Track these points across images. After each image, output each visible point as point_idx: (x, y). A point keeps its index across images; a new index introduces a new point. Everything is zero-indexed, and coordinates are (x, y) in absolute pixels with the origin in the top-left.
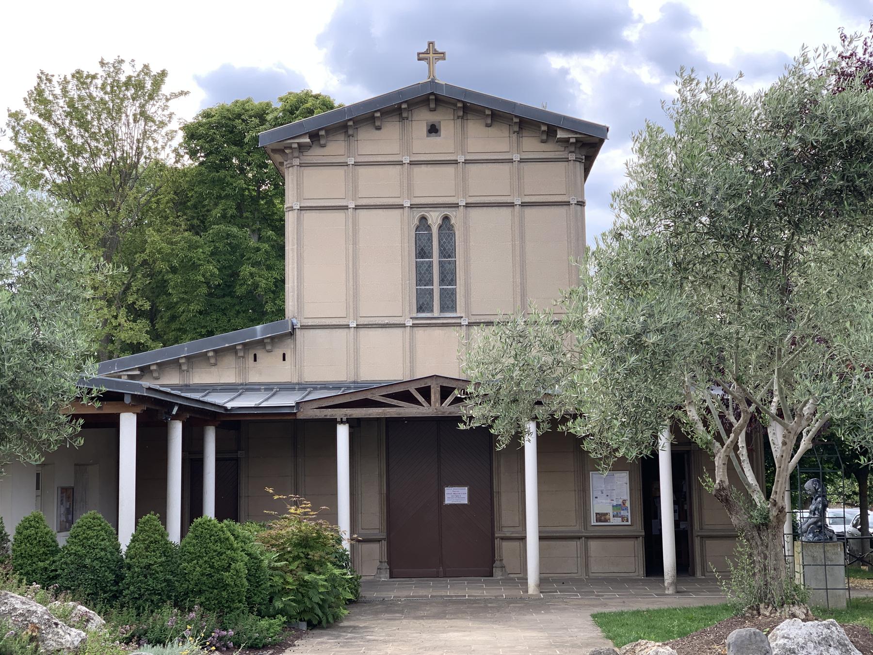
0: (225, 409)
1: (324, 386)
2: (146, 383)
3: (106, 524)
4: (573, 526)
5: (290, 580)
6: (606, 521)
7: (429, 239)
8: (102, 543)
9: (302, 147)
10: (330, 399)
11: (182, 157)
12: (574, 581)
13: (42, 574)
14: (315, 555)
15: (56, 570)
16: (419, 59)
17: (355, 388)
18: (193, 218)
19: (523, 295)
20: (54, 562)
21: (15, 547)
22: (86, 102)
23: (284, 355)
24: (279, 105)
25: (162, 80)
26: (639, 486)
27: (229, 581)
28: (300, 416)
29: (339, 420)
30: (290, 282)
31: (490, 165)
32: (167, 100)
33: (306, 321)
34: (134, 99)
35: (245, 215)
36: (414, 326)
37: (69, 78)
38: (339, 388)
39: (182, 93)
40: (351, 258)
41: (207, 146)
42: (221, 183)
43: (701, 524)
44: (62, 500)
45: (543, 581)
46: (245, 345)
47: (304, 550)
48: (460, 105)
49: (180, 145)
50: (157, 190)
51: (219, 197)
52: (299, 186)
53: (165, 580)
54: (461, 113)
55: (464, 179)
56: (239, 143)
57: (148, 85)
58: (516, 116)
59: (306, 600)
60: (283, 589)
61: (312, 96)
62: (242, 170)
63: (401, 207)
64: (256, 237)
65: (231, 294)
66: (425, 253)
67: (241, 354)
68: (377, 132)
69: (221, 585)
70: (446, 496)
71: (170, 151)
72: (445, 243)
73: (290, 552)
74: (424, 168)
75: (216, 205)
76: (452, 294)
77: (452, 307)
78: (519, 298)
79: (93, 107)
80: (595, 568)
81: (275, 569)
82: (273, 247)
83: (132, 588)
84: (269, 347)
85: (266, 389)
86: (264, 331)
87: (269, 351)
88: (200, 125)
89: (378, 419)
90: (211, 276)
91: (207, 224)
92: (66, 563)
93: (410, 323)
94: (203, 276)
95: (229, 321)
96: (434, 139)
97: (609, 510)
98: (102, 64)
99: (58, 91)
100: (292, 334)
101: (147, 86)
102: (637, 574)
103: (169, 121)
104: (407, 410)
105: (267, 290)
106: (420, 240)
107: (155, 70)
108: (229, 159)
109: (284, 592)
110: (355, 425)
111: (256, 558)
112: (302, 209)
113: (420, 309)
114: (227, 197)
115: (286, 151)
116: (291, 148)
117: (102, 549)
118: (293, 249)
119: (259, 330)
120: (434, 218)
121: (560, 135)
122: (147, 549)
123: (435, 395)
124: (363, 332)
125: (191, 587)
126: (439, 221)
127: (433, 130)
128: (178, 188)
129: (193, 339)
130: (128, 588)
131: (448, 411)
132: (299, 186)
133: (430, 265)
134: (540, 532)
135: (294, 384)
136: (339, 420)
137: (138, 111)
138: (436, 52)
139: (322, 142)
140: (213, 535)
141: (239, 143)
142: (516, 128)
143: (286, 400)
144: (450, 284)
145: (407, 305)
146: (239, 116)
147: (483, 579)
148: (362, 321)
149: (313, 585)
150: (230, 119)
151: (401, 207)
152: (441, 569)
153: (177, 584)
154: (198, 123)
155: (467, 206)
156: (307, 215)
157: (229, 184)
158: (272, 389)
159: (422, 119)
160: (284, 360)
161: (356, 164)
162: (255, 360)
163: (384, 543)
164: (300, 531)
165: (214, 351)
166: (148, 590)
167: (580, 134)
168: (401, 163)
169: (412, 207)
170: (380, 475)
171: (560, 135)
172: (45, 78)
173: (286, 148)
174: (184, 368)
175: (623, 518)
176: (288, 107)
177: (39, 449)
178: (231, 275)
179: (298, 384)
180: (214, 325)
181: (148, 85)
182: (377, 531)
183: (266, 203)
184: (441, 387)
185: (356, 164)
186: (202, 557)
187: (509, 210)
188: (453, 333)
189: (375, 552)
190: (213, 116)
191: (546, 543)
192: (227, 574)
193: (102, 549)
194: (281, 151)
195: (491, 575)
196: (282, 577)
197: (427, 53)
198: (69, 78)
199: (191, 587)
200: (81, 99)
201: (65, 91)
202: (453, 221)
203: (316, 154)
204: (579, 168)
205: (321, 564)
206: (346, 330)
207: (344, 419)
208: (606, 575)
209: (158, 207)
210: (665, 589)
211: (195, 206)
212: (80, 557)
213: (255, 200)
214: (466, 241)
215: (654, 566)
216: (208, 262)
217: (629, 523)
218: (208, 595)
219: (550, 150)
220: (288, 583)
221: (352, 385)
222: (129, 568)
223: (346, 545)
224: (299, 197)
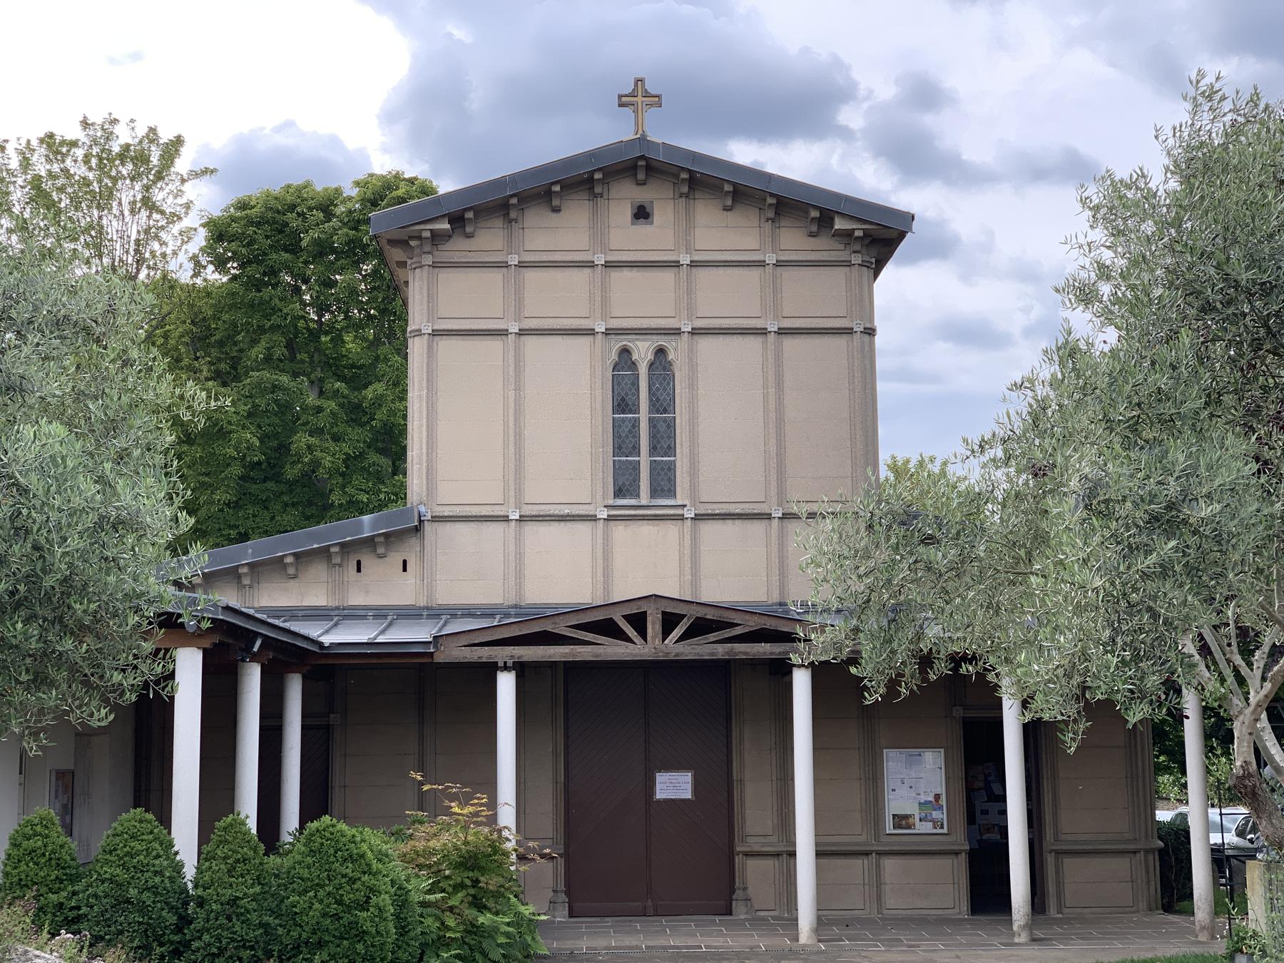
0: (321, 645)
1: (469, 612)
2: (228, 597)
3: (160, 831)
4: (857, 835)
5: (451, 922)
6: (909, 827)
7: (633, 384)
8: (157, 862)
9: (437, 238)
10: (489, 632)
11: (205, 267)
12: (860, 921)
13: (54, 915)
14: (491, 882)
15: (78, 908)
16: (621, 105)
17: (517, 615)
18: (219, 360)
20: (74, 893)
21: (8, 869)
22: (60, 182)
23: (405, 562)
24: (354, 192)
25: (177, 151)
26: (960, 772)
27: (368, 926)
28: (440, 658)
30: (416, 447)
31: (729, 271)
32: (183, 181)
33: (440, 509)
34: (133, 179)
35: (298, 357)
36: (610, 519)
37: (35, 143)
38: (492, 616)
40: (511, 411)
41: (244, 251)
42: (267, 309)
43: (1056, 834)
44: (57, 791)
45: (822, 923)
46: (343, 545)
47: (471, 874)
48: (684, 176)
50: (164, 318)
51: (262, 330)
52: (431, 298)
53: (261, 925)
54: (685, 189)
55: (690, 291)
56: (294, 248)
57: (155, 160)
58: (772, 195)
60: (439, 938)
61: (404, 179)
62: (297, 290)
63: (591, 332)
64: (316, 390)
65: (277, 477)
66: (627, 405)
67: (337, 560)
68: (554, 215)
69: (354, 932)
70: (658, 786)
71: (184, 257)
72: (658, 389)
73: (447, 878)
74: (626, 273)
75: (254, 342)
76: (669, 469)
77: (670, 490)
78: (773, 477)
79: (70, 190)
80: (891, 901)
82: (341, 406)
83: (206, 937)
84: (381, 550)
85: (375, 617)
86: (375, 525)
87: (381, 556)
89: (553, 664)
90: (248, 449)
91: (241, 371)
92: (95, 896)
93: (604, 514)
94: (236, 449)
95: (273, 518)
96: (642, 229)
98: (85, 124)
99: (14, 163)
100: (418, 529)
101: (151, 160)
102: (957, 910)
103: (187, 213)
105: (334, 472)
106: (619, 384)
107: (166, 136)
108: (273, 272)
110: (523, 670)
112: (436, 333)
113: (619, 493)
114: (274, 328)
115: (412, 243)
116: (420, 238)
117: (156, 873)
118: (420, 397)
119: (367, 523)
120: (643, 351)
121: (839, 224)
122: (230, 872)
124: (530, 528)
125: (304, 935)
126: (650, 356)
127: (642, 214)
128: (196, 314)
129: (216, 545)
130: (200, 938)
131: (674, 652)
132: (431, 298)
133: (635, 424)
134: (817, 844)
135: (420, 608)
137: (139, 197)
138: (647, 95)
139: (469, 229)
141: (294, 248)
142: (771, 214)
143: (418, 633)
144: (666, 455)
145: (600, 485)
146: (292, 207)
147: (717, 918)
148: (528, 510)
149: (492, 932)
150: (278, 212)
151: (591, 332)
152: (650, 903)
153: (280, 931)
154: (231, 217)
155: (695, 332)
156: (444, 344)
157: (275, 310)
158: (385, 617)
159: (624, 196)
160: (405, 570)
161: (522, 265)
162: (359, 570)
163: (561, 862)
164: (466, 843)
165: (295, 555)
166: (233, 940)
167: (871, 223)
168: (591, 265)
169: (608, 333)
171: (839, 224)
173: (411, 238)
174: (246, 581)
175: (935, 823)
176: (369, 195)
177: (106, 701)
178: (279, 450)
179: (427, 608)
180: (250, 523)
181: (155, 160)
183: (332, 340)
184: (664, 613)
185: (522, 265)
186: (322, 886)
187: (760, 339)
188: (672, 529)
189: (547, 874)
190: (253, 207)
191: (825, 861)
192: (365, 914)
193: (156, 873)
194: (403, 243)
195: (729, 912)
196: (437, 918)
198: (35, 143)
199: (304, 935)
200: (50, 174)
201: (26, 164)
202: (671, 356)
203: (457, 248)
207: (510, 664)
208: (909, 912)
209: (166, 342)
210: (1013, 935)
211: (221, 344)
212: (120, 885)
213: (314, 335)
214: (692, 386)
215: (988, 894)
216: (244, 427)
217: (945, 831)
218: (333, 949)
219: (824, 247)
220: (448, 928)
221: (512, 611)
222: (201, 903)
224: (432, 314)
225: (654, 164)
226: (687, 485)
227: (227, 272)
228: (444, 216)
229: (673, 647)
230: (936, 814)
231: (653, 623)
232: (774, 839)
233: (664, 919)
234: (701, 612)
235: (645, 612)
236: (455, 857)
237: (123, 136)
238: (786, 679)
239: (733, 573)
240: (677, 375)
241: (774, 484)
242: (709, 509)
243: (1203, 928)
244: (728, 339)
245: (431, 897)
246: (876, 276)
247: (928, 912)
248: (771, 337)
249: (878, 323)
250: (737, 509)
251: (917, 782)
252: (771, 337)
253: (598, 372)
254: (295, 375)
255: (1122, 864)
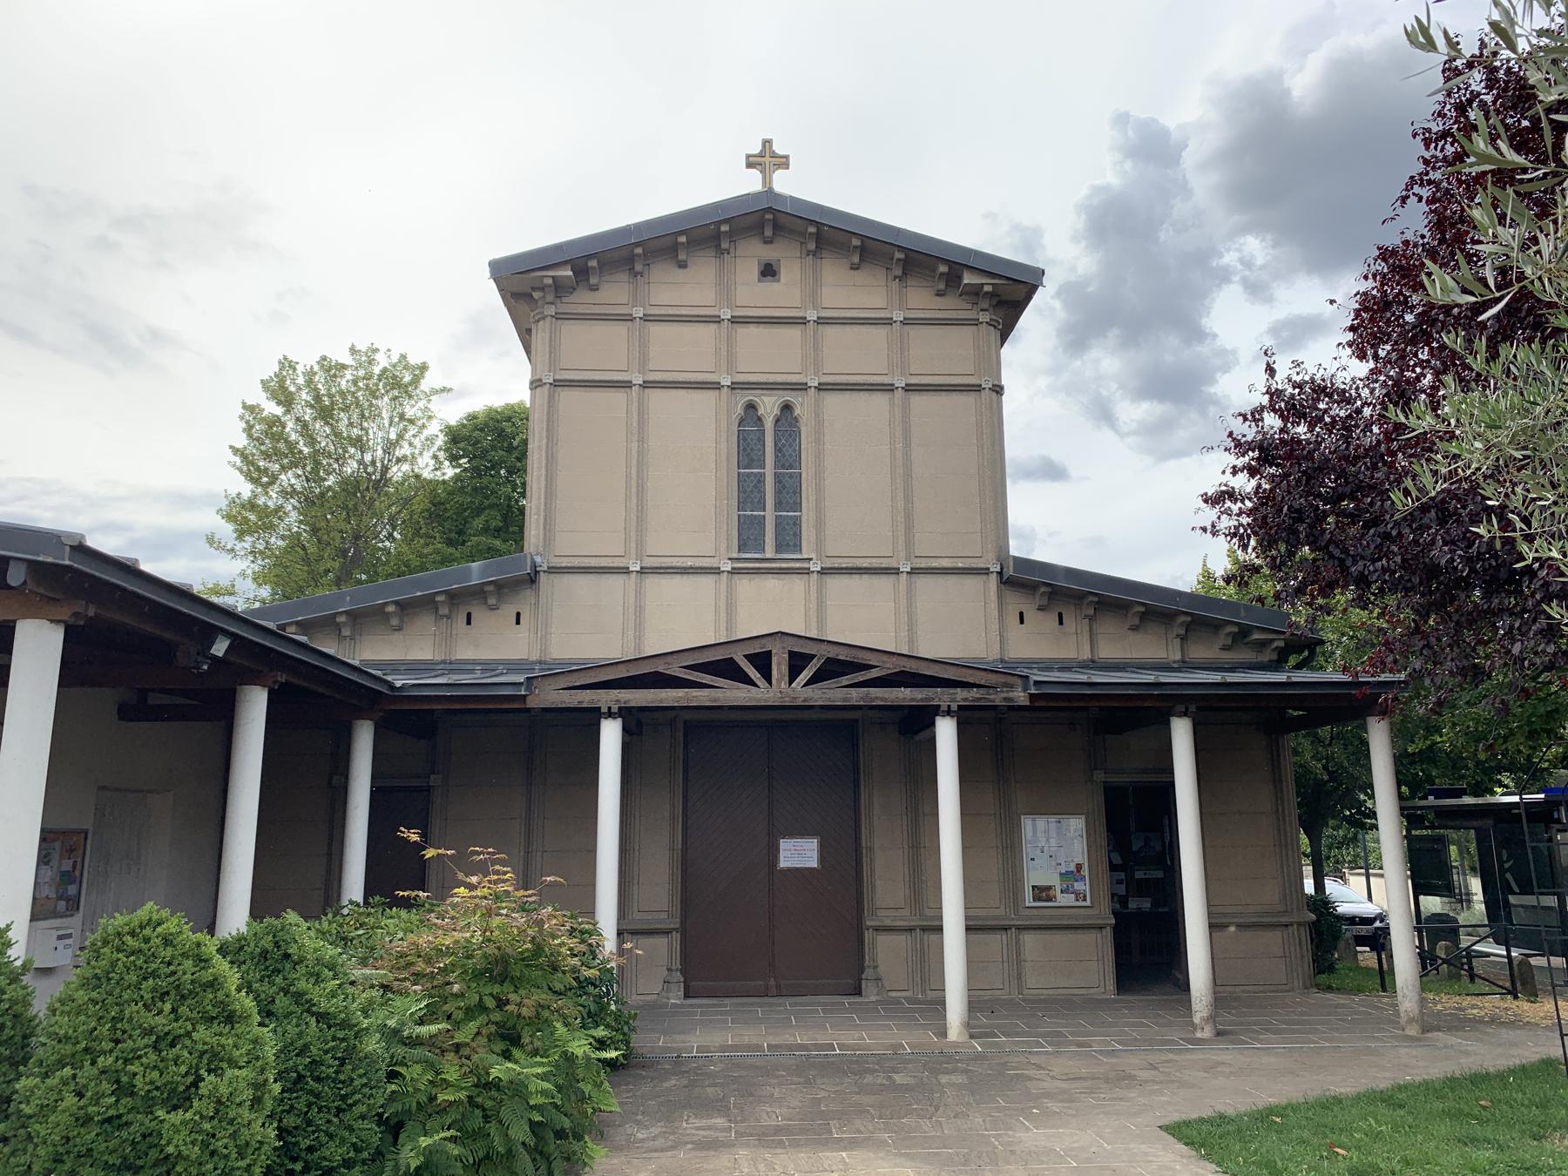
0: (391, 687)
4: (996, 910)
5: (452, 1074)
6: (1049, 899)
10: (592, 673)
14: (524, 1002)
19: (909, 528)
23: (518, 615)
28: (533, 703)
29: (604, 710)
31: (856, 328)
39: (444, 390)
40: (634, 462)
47: (496, 989)
48: (812, 229)
49: (440, 449)
54: (812, 246)
59: (492, 1128)
63: (716, 386)
67: (444, 611)
74: (753, 330)
80: (1032, 981)
81: (415, 1042)
84: (492, 601)
86: (484, 572)
87: (493, 608)
88: (464, 426)
93: (728, 567)
96: (769, 286)
97: (1053, 880)
98: (353, 351)
99: (301, 380)
100: (532, 579)
101: (402, 382)
104: (729, 694)
109: (429, 1110)
111: (345, 1025)
114: (491, 506)
115: (536, 295)
119: (476, 571)
120: (769, 406)
121: (968, 278)
123: (779, 668)
124: (651, 581)
126: (776, 411)
127: (769, 271)
133: (761, 479)
136: (604, 710)
138: (774, 155)
140: (155, 975)
146: (509, 419)
147: (846, 1000)
148: (649, 562)
149: (517, 1089)
151: (716, 386)
152: (772, 982)
155: (821, 388)
159: (752, 253)
160: (518, 622)
161: (646, 318)
162: (469, 623)
163: (676, 936)
165: (396, 603)
168: (716, 320)
169: (734, 387)
170: (673, 818)
171: (968, 278)
172: (287, 365)
174: (346, 632)
179: (540, 662)
182: (664, 916)
184: (791, 653)
188: (798, 583)
189: (663, 950)
195: (858, 992)
196: (430, 1065)
197: (761, 155)
202: (797, 412)
203: (581, 300)
204: (994, 335)
205: (539, 1021)
206: (624, 576)
207: (615, 709)
214: (819, 440)
217: (1088, 903)
219: (952, 306)
220: (446, 1084)
223: (610, 944)
225: (782, 219)
226: (813, 539)
227: (460, 466)
228: (566, 262)
229: (801, 691)
230: (1078, 886)
231: (779, 664)
232: (906, 912)
233: (788, 1001)
234: (833, 652)
235: (770, 652)
236: (477, 962)
237: (382, 362)
238: (923, 735)
239: (864, 619)
240: (803, 430)
241: (902, 539)
242: (836, 563)
243: (1411, 1020)
244: (855, 395)
245: (424, 1030)
246: (1004, 337)
247: (1076, 992)
248: (899, 393)
249: (1005, 381)
250: (865, 563)
251: (1059, 847)
252: (899, 393)
253: (724, 424)
254: (505, 541)
255: (1276, 937)
